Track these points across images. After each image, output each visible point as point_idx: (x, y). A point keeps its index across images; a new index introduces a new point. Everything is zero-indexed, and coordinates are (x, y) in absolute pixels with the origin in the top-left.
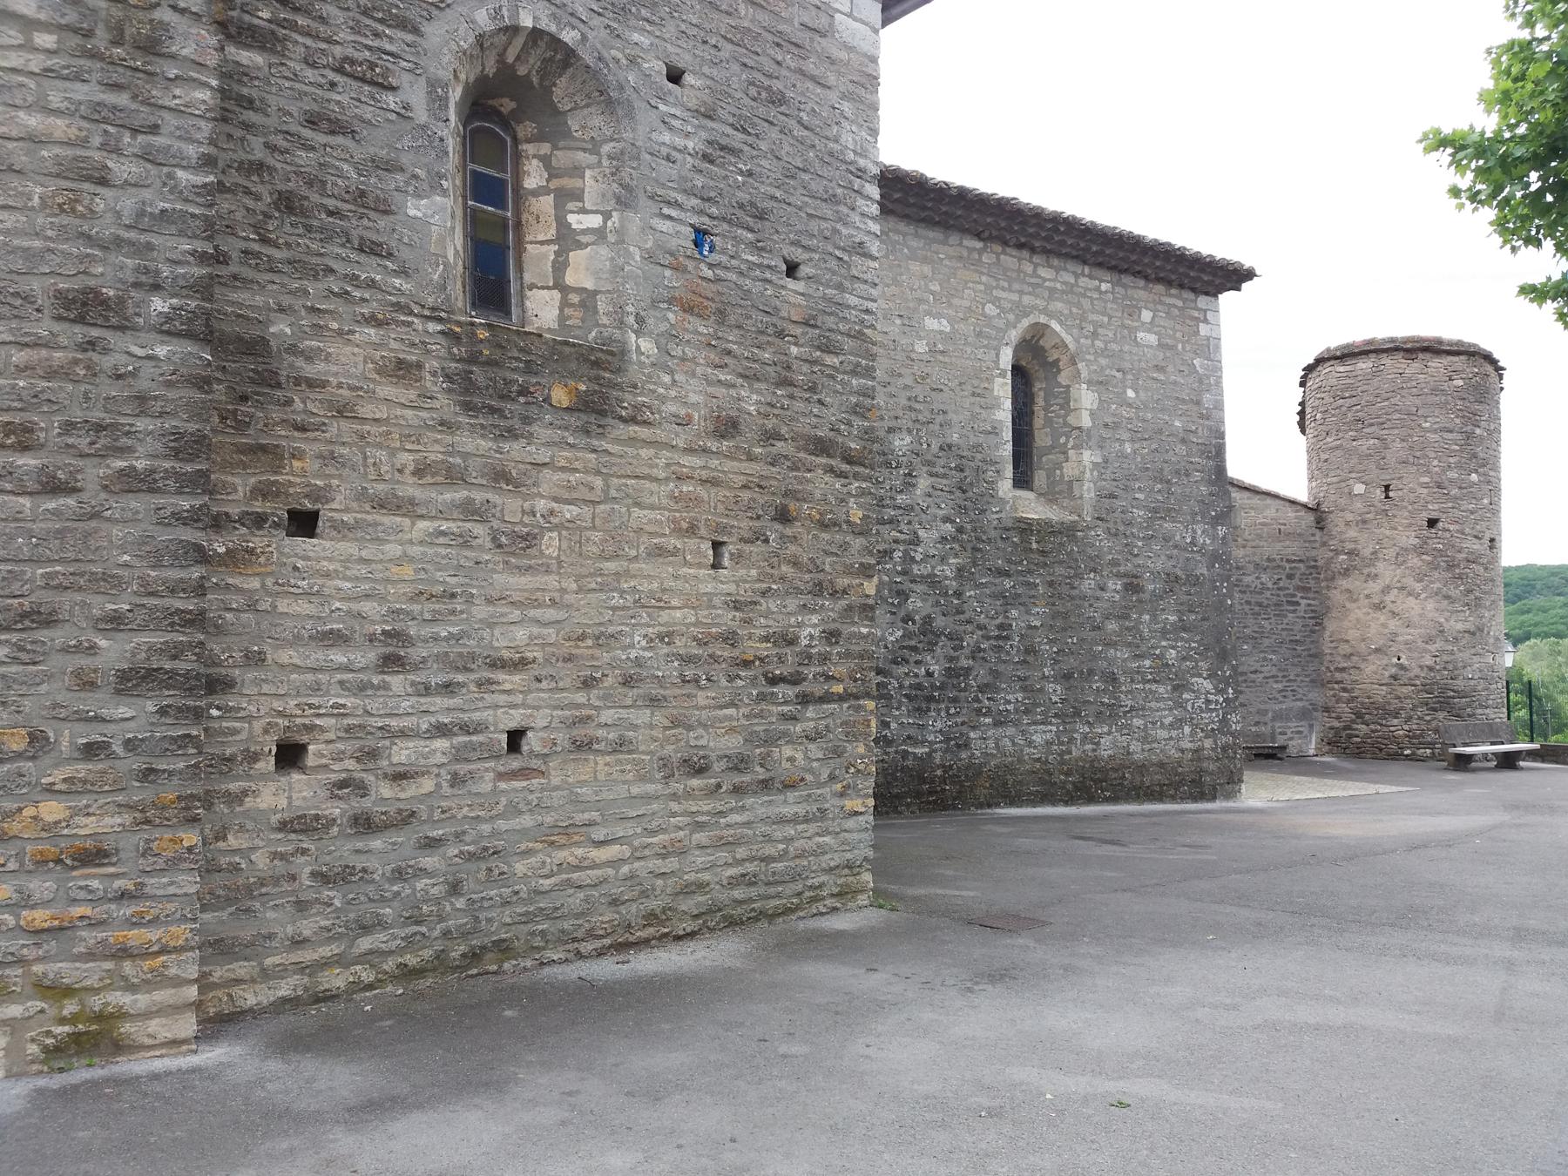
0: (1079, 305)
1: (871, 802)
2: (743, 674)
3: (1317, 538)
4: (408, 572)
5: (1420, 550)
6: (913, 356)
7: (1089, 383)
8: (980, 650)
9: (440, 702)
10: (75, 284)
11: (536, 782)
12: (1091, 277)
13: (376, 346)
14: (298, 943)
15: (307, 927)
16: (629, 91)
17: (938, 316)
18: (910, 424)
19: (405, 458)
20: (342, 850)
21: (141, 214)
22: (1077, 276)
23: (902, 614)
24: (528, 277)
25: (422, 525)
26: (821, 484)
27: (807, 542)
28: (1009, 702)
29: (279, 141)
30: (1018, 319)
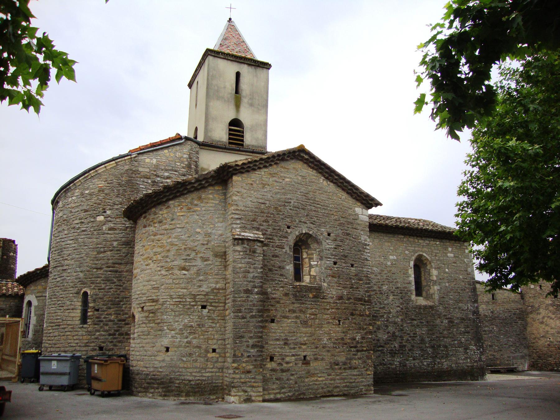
0: (431, 249)
1: (373, 372)
3: (522, 302)
5: (552, 305)
7: (435, 268)
8: (408, 340)
9: (293, 351)
10: (246, 288)
12: (434, 241)
13: (283, 291)
14: (273, 389)
15: (274, 387)
17: (394, 255)
19: (287, 309)
20: (279, 375)
21: (253, 277)
22: (429, 241)
23: (387, 331)
24: (304, 274)
25: (290, 320)
26: (360, 307)
28: (417, 354)
29: (268, 260)
30: (414, 253)
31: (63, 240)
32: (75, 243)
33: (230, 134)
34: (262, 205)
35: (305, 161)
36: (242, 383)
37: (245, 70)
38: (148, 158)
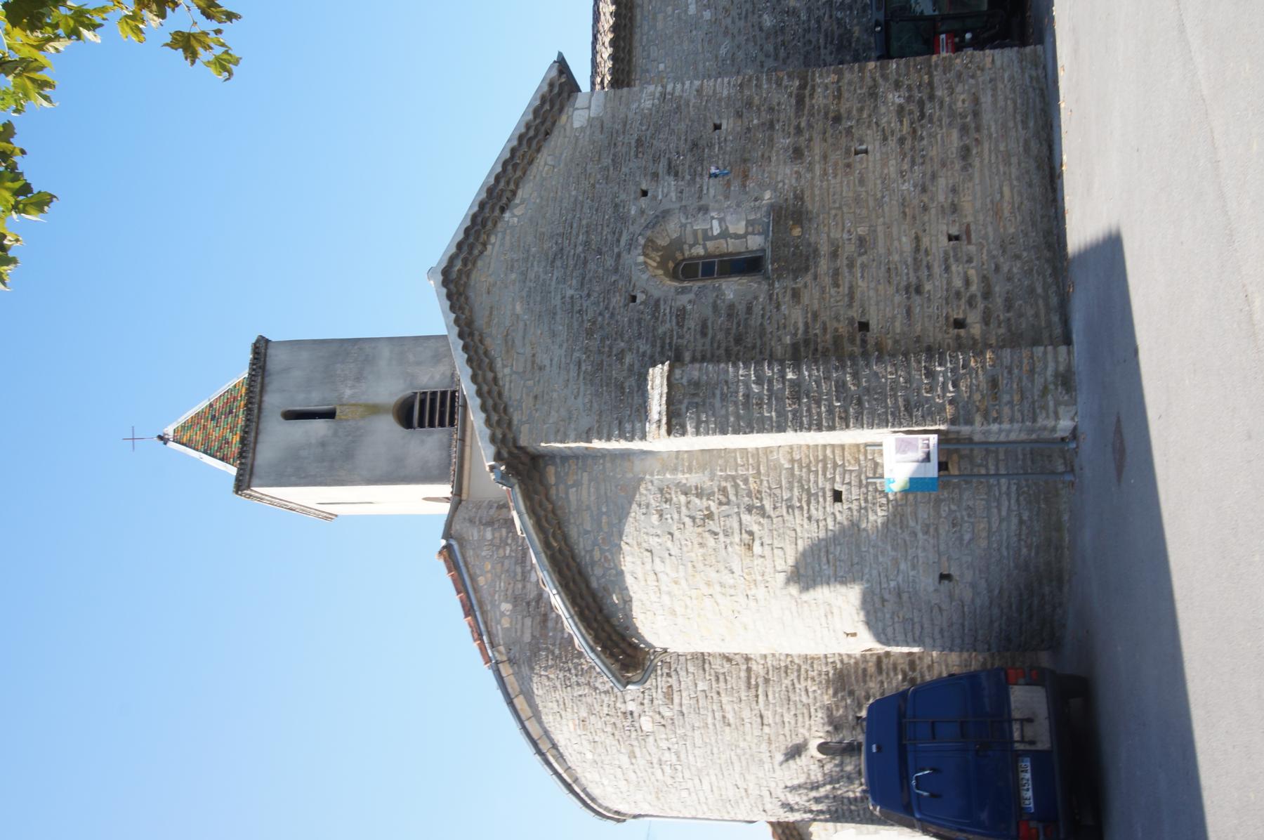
2: (920, 133)
4: (881, 287)
6: (713, 20)
11: (973, 227)
16: (657, 213)
18: (756, 16)
19: (833, 291)
24: (743, 250)
27: (849, 103)
29: (715, 345)
31: (703, 800)
32: (708, 774)
33: (432, 425)
34: (583, 368)
35: (470, 266)
36: (1022, 398)
37: (274, 401)
38: (499, 622)
